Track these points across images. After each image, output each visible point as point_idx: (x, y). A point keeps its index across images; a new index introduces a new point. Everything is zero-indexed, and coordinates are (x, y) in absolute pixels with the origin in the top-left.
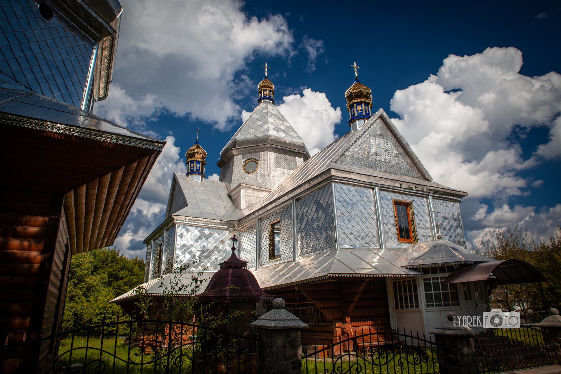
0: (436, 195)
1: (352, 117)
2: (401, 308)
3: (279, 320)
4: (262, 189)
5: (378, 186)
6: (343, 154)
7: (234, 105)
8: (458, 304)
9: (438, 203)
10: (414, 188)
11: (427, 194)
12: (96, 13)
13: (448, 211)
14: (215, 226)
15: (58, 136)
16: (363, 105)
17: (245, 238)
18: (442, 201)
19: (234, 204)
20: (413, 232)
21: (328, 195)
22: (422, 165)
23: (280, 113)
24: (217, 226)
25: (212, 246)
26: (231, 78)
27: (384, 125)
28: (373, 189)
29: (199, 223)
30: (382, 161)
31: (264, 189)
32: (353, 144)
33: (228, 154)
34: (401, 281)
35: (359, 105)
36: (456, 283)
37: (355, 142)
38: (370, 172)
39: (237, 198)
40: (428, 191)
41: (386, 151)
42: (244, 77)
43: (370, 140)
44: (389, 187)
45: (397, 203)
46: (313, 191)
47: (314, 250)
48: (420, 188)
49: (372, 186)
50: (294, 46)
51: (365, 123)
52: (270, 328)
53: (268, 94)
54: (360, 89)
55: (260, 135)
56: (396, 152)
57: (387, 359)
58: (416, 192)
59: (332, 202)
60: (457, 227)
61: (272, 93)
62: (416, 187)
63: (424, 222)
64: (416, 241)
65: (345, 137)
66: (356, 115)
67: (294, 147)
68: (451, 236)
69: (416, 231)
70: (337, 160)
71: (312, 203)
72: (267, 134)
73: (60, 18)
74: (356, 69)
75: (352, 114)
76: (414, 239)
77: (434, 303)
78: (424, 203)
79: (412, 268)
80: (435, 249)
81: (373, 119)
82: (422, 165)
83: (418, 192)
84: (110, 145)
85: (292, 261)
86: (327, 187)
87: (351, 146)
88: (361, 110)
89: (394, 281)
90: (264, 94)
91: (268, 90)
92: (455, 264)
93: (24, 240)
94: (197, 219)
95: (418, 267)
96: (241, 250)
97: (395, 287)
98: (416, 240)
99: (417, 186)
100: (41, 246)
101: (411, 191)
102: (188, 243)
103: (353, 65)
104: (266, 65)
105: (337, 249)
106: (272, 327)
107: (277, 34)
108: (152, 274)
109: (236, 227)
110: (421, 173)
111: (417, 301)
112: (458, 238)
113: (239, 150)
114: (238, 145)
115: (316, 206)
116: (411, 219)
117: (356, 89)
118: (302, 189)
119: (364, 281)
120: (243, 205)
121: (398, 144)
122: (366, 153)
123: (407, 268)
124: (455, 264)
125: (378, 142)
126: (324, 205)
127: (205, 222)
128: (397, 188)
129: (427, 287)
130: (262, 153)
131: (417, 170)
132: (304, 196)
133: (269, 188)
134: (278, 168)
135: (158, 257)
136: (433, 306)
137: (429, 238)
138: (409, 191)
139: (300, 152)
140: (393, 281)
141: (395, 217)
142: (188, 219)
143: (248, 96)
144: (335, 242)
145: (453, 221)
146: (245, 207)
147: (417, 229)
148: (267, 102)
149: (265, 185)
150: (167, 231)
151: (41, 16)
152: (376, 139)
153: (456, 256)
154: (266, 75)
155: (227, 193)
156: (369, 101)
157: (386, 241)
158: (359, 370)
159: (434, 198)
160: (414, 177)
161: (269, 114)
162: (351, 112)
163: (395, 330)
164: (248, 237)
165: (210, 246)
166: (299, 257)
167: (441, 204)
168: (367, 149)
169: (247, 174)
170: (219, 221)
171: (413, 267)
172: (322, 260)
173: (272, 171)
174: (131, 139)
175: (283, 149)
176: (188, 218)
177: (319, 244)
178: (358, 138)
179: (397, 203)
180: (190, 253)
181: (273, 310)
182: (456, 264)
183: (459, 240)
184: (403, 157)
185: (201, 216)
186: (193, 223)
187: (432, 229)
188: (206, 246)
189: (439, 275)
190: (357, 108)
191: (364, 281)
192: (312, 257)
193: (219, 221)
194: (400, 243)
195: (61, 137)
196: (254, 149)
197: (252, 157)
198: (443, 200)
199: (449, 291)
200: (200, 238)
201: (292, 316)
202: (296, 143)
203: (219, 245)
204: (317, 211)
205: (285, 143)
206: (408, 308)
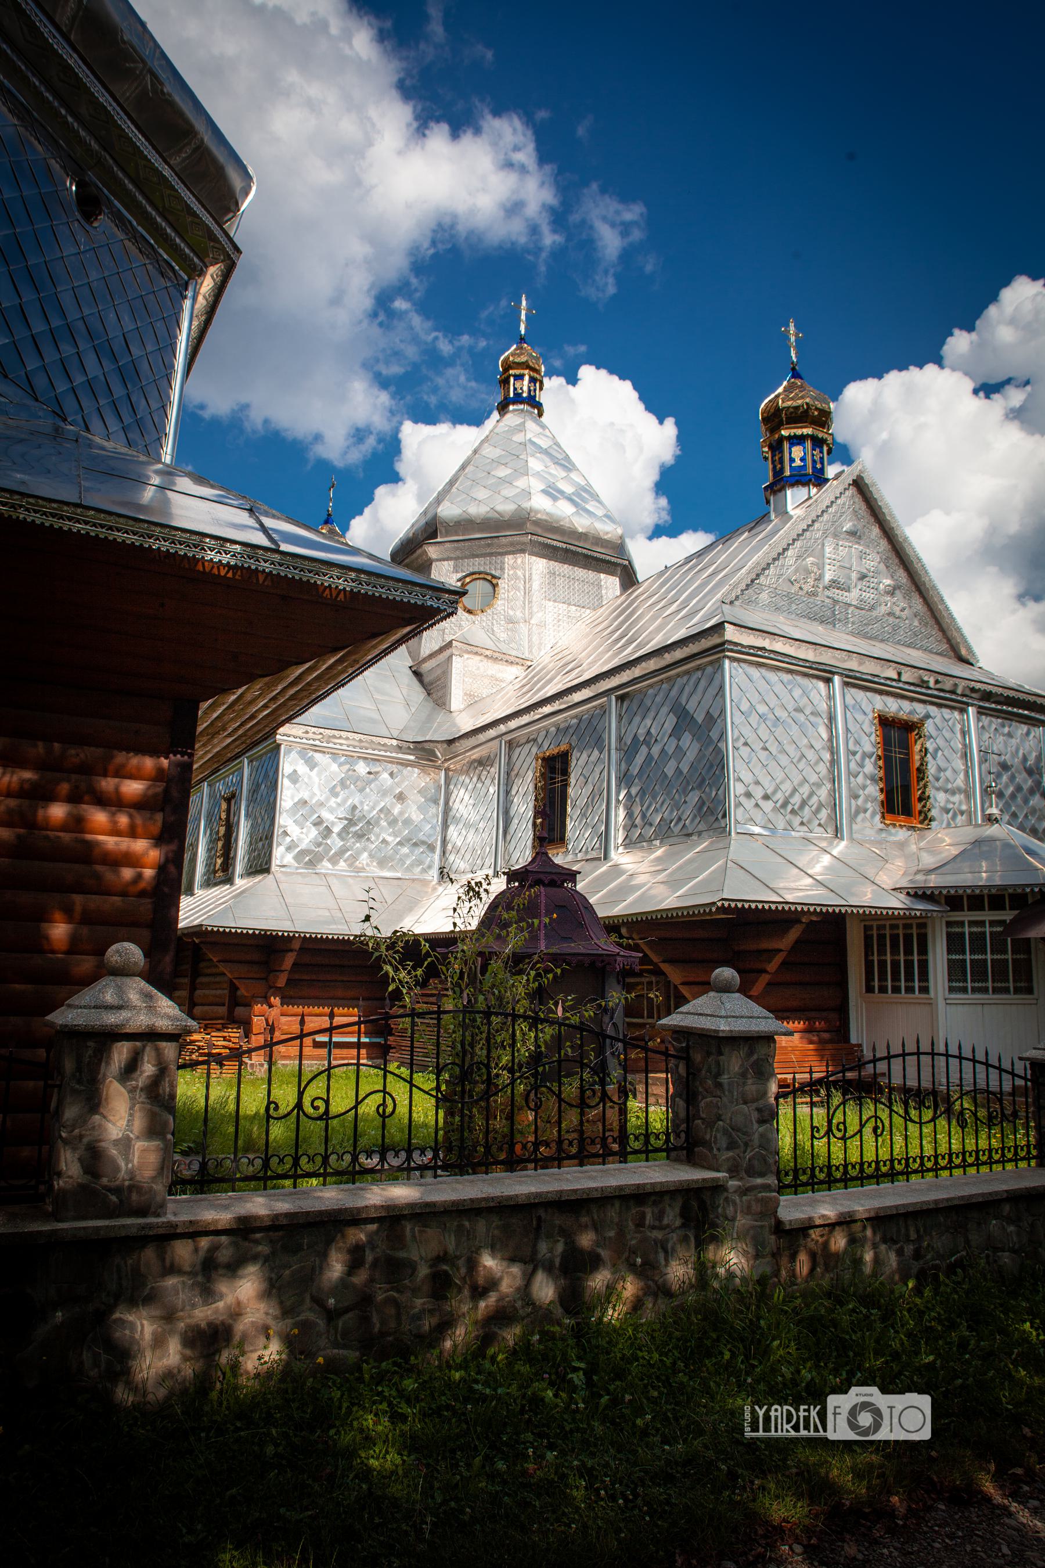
0: (987, 705)
1: (774, 476)
2: (893, 992)
3: (733, 1017)
4: (508, 657)
5: (841, 674)
6: (752, 581)
7: (375, 391)
8: (1030, 991)
9: (990, 725)
10: (932, 684)
11: (964, 699)
12: (200, 202)
13: (1014, 748)
14: (382, 753)
15: (227, 572)
16: (809, 444)
17: (462, 791)
18: (1000, 721)
19: (429, 694)
20: (920, 799)
21: (712, 691)
22: (953, 619)
23: (559, 446)
24: (388, 754)
25: (373, 808)
26: (367, 303)
27: (863, 506)
28: (828, 681)
29: (341, 744)
30: (850, 605)
31: (512, 659)
32: (779, 554)
33: (415, 555)
34: (872, 926)
35: (798, 444)
36: (1029, 939)
37: (785, 550)
38: (818, 632)
39: (438, 679)
40: (968, 692)
41: (863, 577)
42: (400, 304)
43: (823, 545)
44: (869, 677)
45: (885, 722)
46: (669, 679)
47: (664, 833)
48: (948, 684)
49: (825, 674)
50: (559, 217)
51: (810, 498)
52: (721, 1034)
53: (525, 388)
54: (802, 398)
55: (506, 508)
56: (888, 582)
57: (935, 1112)
58: (936, 693)
59: (723, 711)
60: (1032, 792)
61: (538, 385)
62: (937, 682)
63: (949, 773)
64: (926, 822)
65: (754, 532)
66: (787, 473)
67: (597, 544)
68: (1014, 815)
69: (929, 797)
70: (737, 598)
71: (665, 710)
72: (526, 505)
73: (119, 220)
74: (793, 339)
75: (774, 467)
76: (921, 818)
77: (969, 985)
78: (954, 724)
79: (920, 893)
80: (979, 847)
81: (832, 489)
82: (954, 619)
83: (942, 694)
84: (342, 596)
85: (599, 859)
86: (709, 670)
87: (774, 560)
88: (802, 459)
89: (867, 923)
90: (515, 389)
91: (527, 378)
92: (1032, 890)
93: (120, 811)
94: (336, 733)
95: (936, 892)
96: (449, 821)
97: (868, 939)
98: (926, 819)
99: (940, 678)
100: (156, 826)
101: (923, 690)
102: (312, 798)
103: (788, 326)
104: (524, 303)
105: (730, 834)
106: (723, 1031)
107: (502, 175)
108: (205, 875)
109: (437, 757)
110: (949, 641)
111: (924, 975)
112: (1033, 821)
113: (448, 545)
114: (444, 531)
115: (675, 720)
116: (917, 764)
117: (792, 399)
118: (637, 672)
119: (799, 921)
120: (457, 701)
121: (897, 561)
122: (811, 581)
123: (908, 894)
124: (1032, 890)
125: (843, 552)
126: (700, 718)
127: (357, 744)
128: (888, 682)
129: (955, 943)
130: (509, 559)
131: (940, 634)
132: (640, 690)
133: (526, 655)
134: (551, 603)
135: (222, 830)
136: (964, 990)
137: (959, 817)
138: (918, 689)
139: (613, 560)
140: (863, 924)
141: (879, 758)
142: (314, 733)
143: (416, 366)
144: (724, 816)
145: (1024, 775)
146: (462, 707)
147: (930, 791)
148: (522, 410)
149: (516, 647)
150: (251, 761)
151: (79, 217)
152: (841, 543)
153: (1037, 869)
154: (523, 332)
155: (411, 664)
156: (825, 436)
157: (853, 818)
158: (879, 1131)
159: (981, 712)
160: (931, 652)
161: (530, 448)
162: (773, 462)
163: (860, 1046)
164: (470, 787)
165: (369, 804)
166: (621, 849)
167: (996, 729)
168: (815, 570)
169: (467, 615)
170: (395, 742)
171: (924, 893)
172: (691, 861)
173: (535, 609)
174: (391, 583)
175: (566, 550)
176: (314, 729)
177: (680, 819)
178: (794, 540)
179: (885, 722)
180: (318, 823)
181: (712, 994)
182: (1036, 890)
183: (1033, 825)
184: (907, 596)
185: (346, 725)
186: (324, 744)
187: (968, 794)
188: (360, 808)
189: (987, 916)
190: (790, 453)
191: (799, 921)
192: (659, 853)
193: (395, 742)
194: (888, 825)
195: (234, 574)
196: (489, 545)
197: (482, 569)
198: (1003, 718)
199: (1009, 956)
200: (343, 783)
201: (758, 1010)
202: (601, 534)
203: (393, 805)
204: (676, 732)
205: (574, 533)
206: (873, 992)
